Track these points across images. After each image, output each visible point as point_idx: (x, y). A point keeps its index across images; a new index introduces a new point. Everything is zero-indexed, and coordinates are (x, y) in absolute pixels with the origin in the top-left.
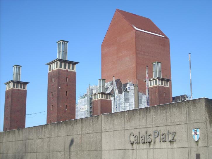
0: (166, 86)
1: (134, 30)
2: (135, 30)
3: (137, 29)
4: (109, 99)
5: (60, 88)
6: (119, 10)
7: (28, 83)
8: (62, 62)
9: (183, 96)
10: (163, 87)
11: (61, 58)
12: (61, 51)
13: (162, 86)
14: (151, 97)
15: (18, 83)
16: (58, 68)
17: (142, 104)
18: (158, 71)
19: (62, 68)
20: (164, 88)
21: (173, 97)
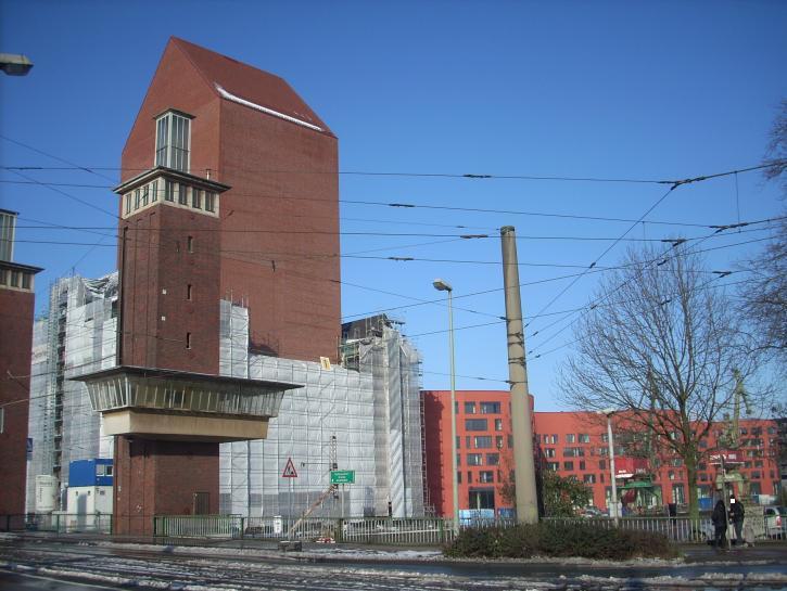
0: (203, 211)
1: (218, 99)
2: (221, 97)
3: (226, 94)
4: (25, 290)
5: (164, 292)
6: (179, 39)
7: (37, 270)
8: (172, 183)
9: (374, 318)
10: (187, 211)
11: (169, 166)
12: (169, 143)
13: (196, 210)
14: (136, 256)
15: (18, 272)
16: (160, 199)
17: (227, 337)
18: (186, 151)
19: (172, 200)
20: (193, 216)
21: (345, 321)
